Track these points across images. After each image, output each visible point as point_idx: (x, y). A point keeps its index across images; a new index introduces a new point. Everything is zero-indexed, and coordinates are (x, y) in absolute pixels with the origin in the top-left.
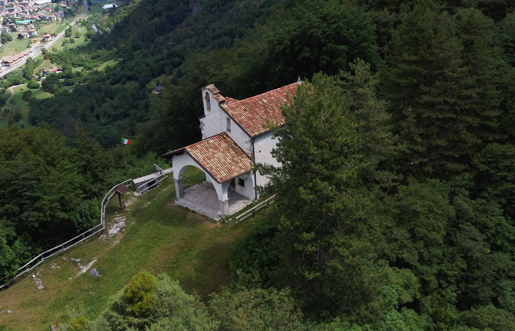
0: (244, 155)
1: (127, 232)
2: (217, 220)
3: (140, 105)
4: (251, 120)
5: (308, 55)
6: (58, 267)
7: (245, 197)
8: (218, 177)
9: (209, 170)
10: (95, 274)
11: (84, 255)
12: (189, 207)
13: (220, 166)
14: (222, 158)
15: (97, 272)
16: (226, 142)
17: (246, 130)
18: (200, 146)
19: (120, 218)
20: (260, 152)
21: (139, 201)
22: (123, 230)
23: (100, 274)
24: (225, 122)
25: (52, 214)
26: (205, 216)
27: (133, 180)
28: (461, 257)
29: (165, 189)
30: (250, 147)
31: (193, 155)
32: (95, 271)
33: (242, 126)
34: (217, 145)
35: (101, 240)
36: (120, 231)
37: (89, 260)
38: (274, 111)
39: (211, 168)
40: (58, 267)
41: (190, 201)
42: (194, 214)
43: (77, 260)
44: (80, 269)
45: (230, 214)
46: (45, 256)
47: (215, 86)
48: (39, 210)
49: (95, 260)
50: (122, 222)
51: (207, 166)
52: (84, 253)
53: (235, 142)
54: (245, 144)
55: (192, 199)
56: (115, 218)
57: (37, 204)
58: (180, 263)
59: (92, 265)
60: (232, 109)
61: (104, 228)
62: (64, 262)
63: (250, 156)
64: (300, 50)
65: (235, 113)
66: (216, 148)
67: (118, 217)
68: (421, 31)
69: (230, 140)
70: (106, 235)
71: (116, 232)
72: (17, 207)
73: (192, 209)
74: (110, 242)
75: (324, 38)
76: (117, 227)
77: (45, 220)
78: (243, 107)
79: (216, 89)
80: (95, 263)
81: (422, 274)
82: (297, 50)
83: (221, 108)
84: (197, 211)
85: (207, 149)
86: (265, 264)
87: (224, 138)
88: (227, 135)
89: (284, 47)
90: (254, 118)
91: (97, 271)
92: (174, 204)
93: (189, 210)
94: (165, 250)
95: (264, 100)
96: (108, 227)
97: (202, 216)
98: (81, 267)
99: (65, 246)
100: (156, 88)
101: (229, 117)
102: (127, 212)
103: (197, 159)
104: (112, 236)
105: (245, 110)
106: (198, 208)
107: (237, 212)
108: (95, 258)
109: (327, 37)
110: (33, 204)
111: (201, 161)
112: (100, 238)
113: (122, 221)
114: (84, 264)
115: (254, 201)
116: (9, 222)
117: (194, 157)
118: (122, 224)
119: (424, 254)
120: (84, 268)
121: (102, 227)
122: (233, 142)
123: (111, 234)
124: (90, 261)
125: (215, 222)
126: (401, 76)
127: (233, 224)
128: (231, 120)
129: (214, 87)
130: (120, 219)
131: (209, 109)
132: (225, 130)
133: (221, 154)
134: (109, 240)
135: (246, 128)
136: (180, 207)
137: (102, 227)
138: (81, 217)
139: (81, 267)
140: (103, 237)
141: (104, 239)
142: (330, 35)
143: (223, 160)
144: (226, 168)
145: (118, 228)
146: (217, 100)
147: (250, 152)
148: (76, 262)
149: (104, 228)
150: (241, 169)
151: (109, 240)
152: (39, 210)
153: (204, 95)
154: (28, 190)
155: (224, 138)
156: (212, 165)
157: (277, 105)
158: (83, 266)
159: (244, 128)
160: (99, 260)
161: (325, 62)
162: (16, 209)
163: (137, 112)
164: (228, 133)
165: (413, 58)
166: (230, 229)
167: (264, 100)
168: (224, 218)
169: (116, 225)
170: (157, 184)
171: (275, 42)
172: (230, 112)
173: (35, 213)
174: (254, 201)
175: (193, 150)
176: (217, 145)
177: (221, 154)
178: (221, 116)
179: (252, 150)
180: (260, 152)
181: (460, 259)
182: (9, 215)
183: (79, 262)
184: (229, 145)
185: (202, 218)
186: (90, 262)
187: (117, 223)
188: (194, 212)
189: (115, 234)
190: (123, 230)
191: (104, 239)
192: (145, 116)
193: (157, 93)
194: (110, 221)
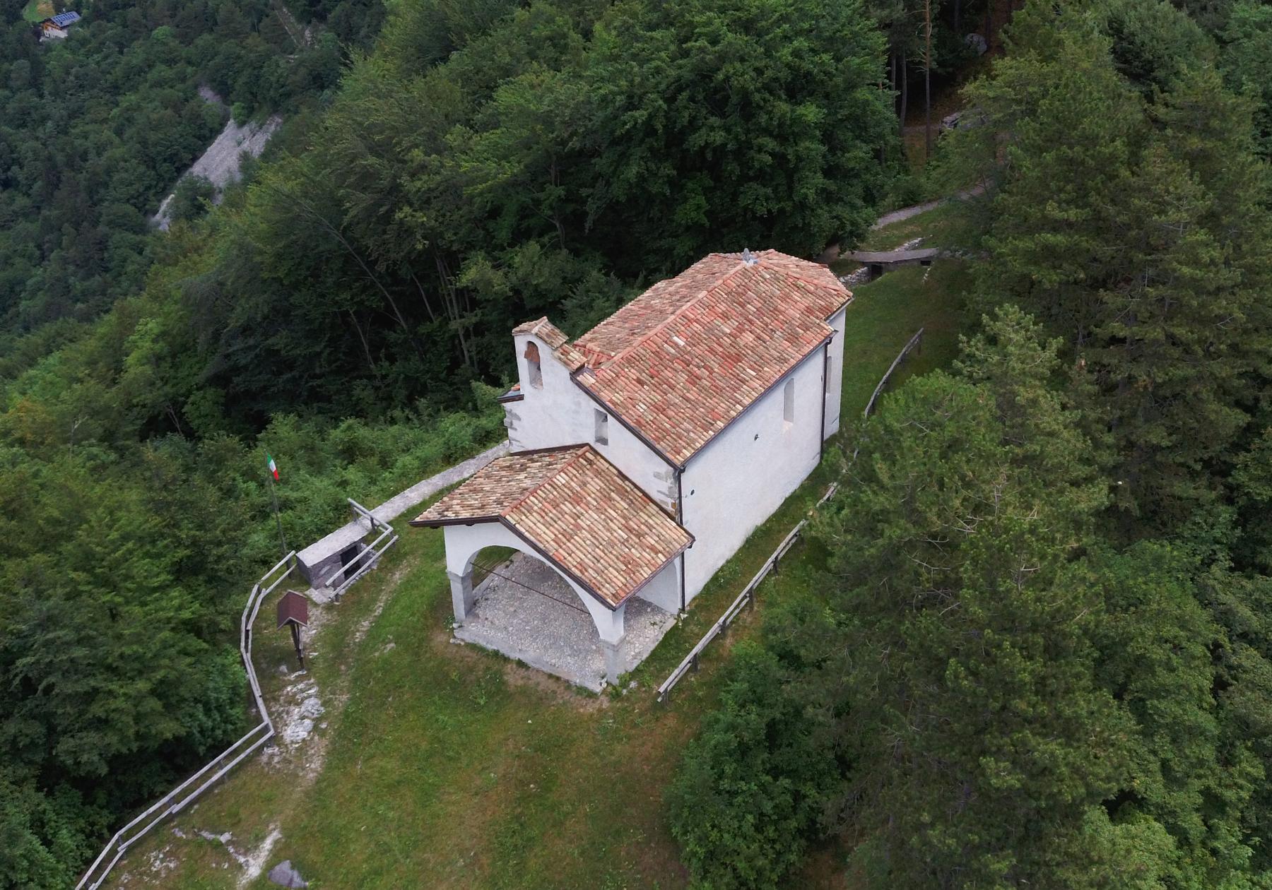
0: (652, 508)
1: (334, 730)
2: (598, 689)
3: (13, 75)
4: (663, 411)
5: (718, 137)
6: (172, 865)
7: (650, 604)
8: (606, 591)
9: (578, 573)
10: (291, 880)
11: (239, 821)
12: (504, 650)
13: (602, 555)
14: (600, 527)
15: (296, 874)
16: (598, 473)
17: (658, 447)
18: (536, 502)
19: (301, 686)
20: (692, 493)
21: (333, 618)
22: (324, 726)
23: (306, 880)
24: (591, 420)
25: (143, 730)
26: (558, 679)
27: (298, 555)
28: (1247, 748)
29: (397, 575)
30: (670, 488)
31: (527, 534)
32: (290, 872)
33: (648, 438)
34: (578, 489)
35: (269, 763)
36: (315, 728)
37: (257, 836)
38: (711, 371)
39: (583, 568)
40: (172, 865)
41: (498, 629)
42: (522, 672)
43: (224, 838)
44: (241, 866)
45: (631, 668)
46: (123, 839)
47: (551, 320)
48: (102, 724)
49: (275, 835)
50: (312, 701)
51: (571, 562)
52: (237, 815)
53: (620, 472)
54: (656, 480)
55: (503, 622)
56: (285, 686)
57: (97, 710)
58: (535, 832)
59: (271, 851)
60: (609, 384)
61: (271, 733)
62: (178, 844)
63: (670, 509)
64: (693, 126)
65: (618, 398)
66: (577, 499)
67: (294, 683)
68: (1091, 140)
69: (607, 465)
70: (279, 745)
71: (303, 734)
72: (37, 723)
73: (515, 656)
74: (296, 767)
75: (758, 90)
76: (303, 718)
77: (124, 750)
78: (633, 374)
79: (557, 331)
80: (276, 842)
81: (1173, 813)
82: (685, 121)
83: (580, 385)
84: (531, 664)
85: (556, 506)
86: (766, 819)
87: (590, 462)
88: (596, 453)
89: (650, 114)
90: (670, 404)
91: (293, 868)
92: (455, 637)
93: (506, 659)
94: (477, 794)
95: (675, 339)
96: (278, 719)
97: (550, 676)
98: (242, 859)
99: (176, 800)
100: (55, 18)
101: (602, 410)
102: (312, 662)
103: (541, 546)
104: (296, 749)
105: (639, 381)
106: (529, 652)
107: (645, 656)
108: (272, 826)
109: (767, 88)
110: (81, 714)
111: (552, 548)
112: (264, 759)
113: (310, 696)
114: (250, 847)
115: (679, 616)
116: (23, 771)
117: (532, 539)
118: (312, 705)
119: (1172, 764)
120: (251, 861)
121: (266, 729)
122: (616, 472)
123: (292, 742)
124: (260, 838)
125: (591, 695)
126: (1033, 258)
127: (644, 700)
128: (609, 416)
129: (550, 326)
130: (302, 691)
131: (536, 379)
132: (589, 438)
133: (596, 517)
134: (290, 762)
135: (658, 439)
136: (474, 647)
137: (266, 729)
138: (207, 711)
139: (242, 859)
140: (272, 756)
141: (276, 759)
142: (776, 80)
143: (605, 535)
144: (617, 558)
145: (307, 722)
146: (566, 364)
147: (670, 501)
148: (221, 844)
149: (271, 733)
150: (656, 553)
151: (290, 762)
152: (102, 724)
153: (520, 344)
154: (65, 674)
155: (590, 462)
156: (583, 557)
157: (712, 351)
158: (245, 854)
159: (652, 441)
160: (288, 833)
161: (768, 159)
162: (36, 729)
163: (8, 98)
164: (599, 448)
165: (1072, 214)
166: (641, 715)
167: (675, 339)
168: (616, 682)
169: (296, 711)
170: (367, 557)
171: (618, 98)
172: (606, 395)
173: (92, 737)
174: (679, 616)
175: (523, 517)
176: (578, 489)
177: (596, 517)
178: (579, 404)
179: (677, 496)
180: (692, 493)
181: (1247, 753)
182: (15, 751)
183: (229, 842)
184: (609, 482)
185: (552, 685)
186: (263, 839)
187: (298, 704)
188: (521, 664)
189: (304, 740)
190: (324, 726)
191: (276, 759)
192: (36, 108)
193: (63, 34)
194: (276, 700)
